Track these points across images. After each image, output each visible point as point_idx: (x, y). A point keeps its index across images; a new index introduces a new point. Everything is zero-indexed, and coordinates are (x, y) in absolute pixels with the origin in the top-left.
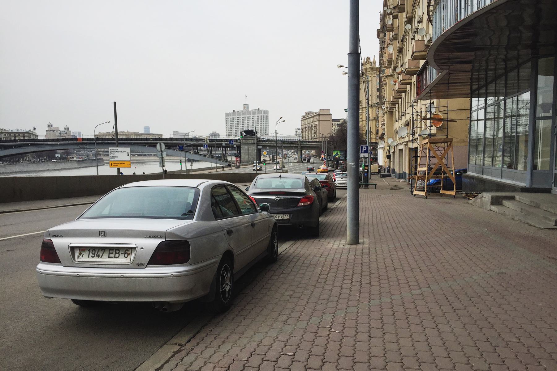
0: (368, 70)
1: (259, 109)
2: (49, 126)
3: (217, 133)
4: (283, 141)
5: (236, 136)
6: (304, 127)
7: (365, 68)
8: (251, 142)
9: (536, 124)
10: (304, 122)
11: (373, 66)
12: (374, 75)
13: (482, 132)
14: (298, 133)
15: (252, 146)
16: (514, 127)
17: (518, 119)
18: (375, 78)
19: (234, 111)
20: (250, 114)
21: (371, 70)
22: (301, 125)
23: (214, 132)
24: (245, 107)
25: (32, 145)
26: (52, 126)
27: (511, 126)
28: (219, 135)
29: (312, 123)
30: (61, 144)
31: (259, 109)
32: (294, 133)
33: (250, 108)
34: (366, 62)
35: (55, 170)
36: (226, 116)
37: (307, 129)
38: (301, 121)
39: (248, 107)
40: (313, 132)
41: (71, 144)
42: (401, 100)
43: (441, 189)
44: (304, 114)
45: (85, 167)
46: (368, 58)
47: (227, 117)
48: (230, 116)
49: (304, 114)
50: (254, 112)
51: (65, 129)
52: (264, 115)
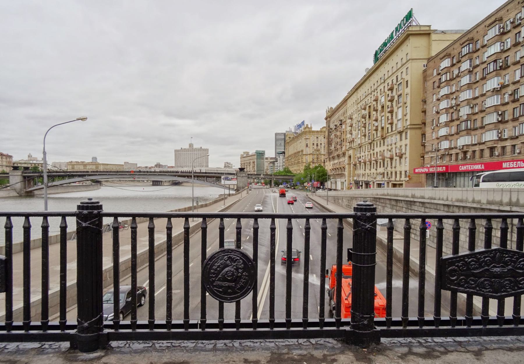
1: (201, 148)
2: (29, 156)
3: (161, 164)
5: (183, 167)
6: (243, 162)
8: (244, 175)
9: (64, 168)
10: (242, 159)
13: (140, 222)
16: (365, 178)
17: (27, 326)
24: (190, 146)
25: (99, 175)
26: (31, 156)
27: (4, 155)
31: (201, 148)
32: (224, 166)
33: (195, 147)
36: (175, 152)
37: (246, 164)
39: (193, 146)
40: (251, 166)
41: (96, 175)
42: (444, 257)
43: (101, 333)
48: (188, 151)
49: (243, 153)
50: (196, 149)
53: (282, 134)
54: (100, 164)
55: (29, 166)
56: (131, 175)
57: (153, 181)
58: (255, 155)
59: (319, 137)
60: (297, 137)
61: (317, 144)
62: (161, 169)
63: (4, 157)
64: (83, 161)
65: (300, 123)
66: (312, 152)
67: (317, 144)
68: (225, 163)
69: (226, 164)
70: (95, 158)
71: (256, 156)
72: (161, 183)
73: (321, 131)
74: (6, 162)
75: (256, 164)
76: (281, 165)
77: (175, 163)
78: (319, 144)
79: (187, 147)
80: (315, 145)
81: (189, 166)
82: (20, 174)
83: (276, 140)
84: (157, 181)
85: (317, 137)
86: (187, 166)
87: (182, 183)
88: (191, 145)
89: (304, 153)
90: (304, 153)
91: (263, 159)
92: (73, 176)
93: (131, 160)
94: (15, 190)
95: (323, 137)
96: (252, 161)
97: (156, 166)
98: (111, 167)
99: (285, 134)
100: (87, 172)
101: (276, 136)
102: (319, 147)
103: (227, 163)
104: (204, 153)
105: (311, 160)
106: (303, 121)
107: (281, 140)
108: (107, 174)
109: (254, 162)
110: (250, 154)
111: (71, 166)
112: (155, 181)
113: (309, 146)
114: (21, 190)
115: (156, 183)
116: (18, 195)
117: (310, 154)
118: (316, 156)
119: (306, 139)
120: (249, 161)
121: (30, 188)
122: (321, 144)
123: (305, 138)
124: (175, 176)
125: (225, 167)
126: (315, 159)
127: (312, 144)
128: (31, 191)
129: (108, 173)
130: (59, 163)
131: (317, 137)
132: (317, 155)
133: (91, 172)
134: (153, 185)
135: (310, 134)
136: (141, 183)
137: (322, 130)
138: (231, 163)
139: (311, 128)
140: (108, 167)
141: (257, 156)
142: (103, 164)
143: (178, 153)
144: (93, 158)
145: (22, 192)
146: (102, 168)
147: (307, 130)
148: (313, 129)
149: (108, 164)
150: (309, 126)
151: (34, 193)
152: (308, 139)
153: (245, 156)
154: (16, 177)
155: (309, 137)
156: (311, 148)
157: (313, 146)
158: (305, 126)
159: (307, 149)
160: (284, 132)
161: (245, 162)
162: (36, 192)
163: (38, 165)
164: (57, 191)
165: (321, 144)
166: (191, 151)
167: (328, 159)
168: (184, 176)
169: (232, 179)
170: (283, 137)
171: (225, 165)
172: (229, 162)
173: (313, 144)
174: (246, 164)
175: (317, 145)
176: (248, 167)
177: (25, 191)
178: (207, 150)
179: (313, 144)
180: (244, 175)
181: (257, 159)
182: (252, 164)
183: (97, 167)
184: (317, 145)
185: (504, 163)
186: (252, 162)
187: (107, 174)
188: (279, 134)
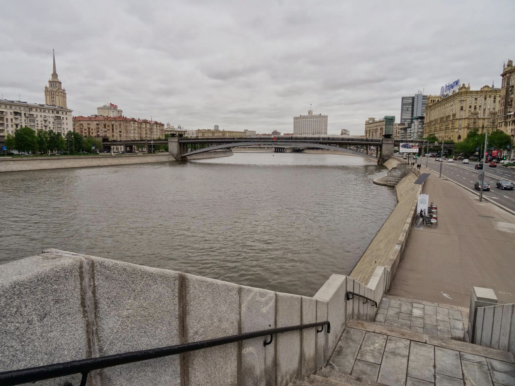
0: (463, 93)
1: (320, 114)
3: (278, 131)
4: (333, 139)
5: (301, 134)
6: (368, 129)
7: (461, 91)
8: (390, 142)
10: (367, 125)
11: (467, 90)
12: (468, 96)
14: (343, 133)
15: (390, 145)
18: (469, 98)
19: (301, 116)
20: (314, 118)
21: (466, 93)
22: (364, 127)
23: (275, 131)
24: (309, 113)
25: (244, 141)
26: (169, 125)
27: (158, 124)
28: (279, 133)
29: (377, 127)
30: (263, 141)
31: (320, 114)
34: (462, 87)
35: (209, 158)
36: (294, 119)
37: (372, 131)
38: (365, 124)
39: (312, 113)
41: (241, 142)
44: (368, 120)
45: (227, 156)
46: (464, 84)
47: (295, 120)
49: (368, 120)
51: (178, 128)
52: (325, 119)
53: (410, 97)
54: (227, 132)
55: (175, 133)
56: (273, 142)
57: (276, 148)
58: (384, 121)
59: (478, 99)
60: (445, 100)
61: (475, 106)
62: (277, 136)
63: (158, 125)
64: (209, 129)
65: (451, 82)
66: (467, 116)
67: (475, 106)
68: (342, 130)
69: (343, 131)
70: (216, 127)
71: (384, 123)
72: (284, 150)
73: (481, 92)
74: (160, 130)
75: (384, 130)
76: (416, 131)
77: (294, 130)
78: (478, 107)
79: (306, 114)
80: (473, 107)
81: (307, 133)
82: (177, 140)
83: (403, 104)
84: (280, 148)
85: (476, 99)
86: (305, 134)
87: (303, 150)
88: (310, 112)
89: (458, 117)
90: (458, 117)
91: (393, 125)
92: (212, 143)
93: (250, 129)
94: (173, 155)
95: (484, 98)
96: (379, 128)
97: (273, 133)
98: (236, 134)
99: (413, 98)
100: (234, 139)
101: (402, 100)
102: (477, 110)
103: (344, 130)
104: (323, 119)
105: (466, 125)
106: (456, 80)
107: (409, 104)
108: (251, 141)
109: (381, 129)
110: (377, 119)
111: (201, 134)
112: (278, 148)
113: (464, 109)
114: (177, 155)
115: (278, 150)
116: (175, 160)
117: (465, 119)
118: (472, 121)
119: (461, 101)
120: (376, 128)
121: (184, 153)
122: (480, 106)
123: (460, 99)
124: (317, 143)
125: (342, 134)
126: (471, 125)
127: (468, 107)
128: (185, 157)
129: (242, 140)
130: (192, 131)
131: (476, 99)
132: (475, 119)
133: (237, 139)
134: (276, 152)
135: (467, 95)
136: (246, 150)
137: (483, 90)
138: (348, 130)
139: (469, 88)
140: (234, 134)
141: (386, 122)
142: (229, 132)
143: (297, 120)
144: (215, 126)
145: (179, 157)
146: (227, 135)
147: (463, 90)
148: (471, 90)
149: (233, 132)
150: (467, 86)
151: (187, 158)
152: (463, 101)
153: (371, 123)
154: (174, 143)
155: (465, 99)
156: (467, 112)
157: (470, 109)
158: (461, 86)
159: (462, 112)
160: (413, 95)
161: (371, 129)
162: (188, 158)
163: (176, 133)
164: (203, 157)
165: (480, 106)
166: (310, 118)
167: (503, 123)
168: (326, 143)
169: (412, 146)
170: (410, 101)
171: (342, 132)
172: (345, 129)
173: (470, 107)
174: (372, 131)
175: (475, 108)
176: (374, 134)
177: (180, 156)
178: (326, 117)
179: (470, 107)
180: (390, 142)
181: (386, 125)
182: (379, 131)
183: (224, 135)
184: (475, 108)
185: (164, 139)
186: (379, 129)
187: (251, 141)
188: (406, 98)
